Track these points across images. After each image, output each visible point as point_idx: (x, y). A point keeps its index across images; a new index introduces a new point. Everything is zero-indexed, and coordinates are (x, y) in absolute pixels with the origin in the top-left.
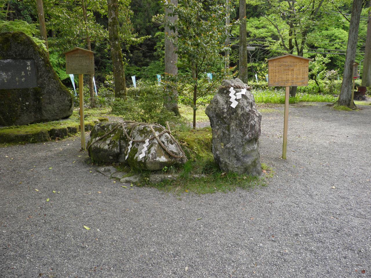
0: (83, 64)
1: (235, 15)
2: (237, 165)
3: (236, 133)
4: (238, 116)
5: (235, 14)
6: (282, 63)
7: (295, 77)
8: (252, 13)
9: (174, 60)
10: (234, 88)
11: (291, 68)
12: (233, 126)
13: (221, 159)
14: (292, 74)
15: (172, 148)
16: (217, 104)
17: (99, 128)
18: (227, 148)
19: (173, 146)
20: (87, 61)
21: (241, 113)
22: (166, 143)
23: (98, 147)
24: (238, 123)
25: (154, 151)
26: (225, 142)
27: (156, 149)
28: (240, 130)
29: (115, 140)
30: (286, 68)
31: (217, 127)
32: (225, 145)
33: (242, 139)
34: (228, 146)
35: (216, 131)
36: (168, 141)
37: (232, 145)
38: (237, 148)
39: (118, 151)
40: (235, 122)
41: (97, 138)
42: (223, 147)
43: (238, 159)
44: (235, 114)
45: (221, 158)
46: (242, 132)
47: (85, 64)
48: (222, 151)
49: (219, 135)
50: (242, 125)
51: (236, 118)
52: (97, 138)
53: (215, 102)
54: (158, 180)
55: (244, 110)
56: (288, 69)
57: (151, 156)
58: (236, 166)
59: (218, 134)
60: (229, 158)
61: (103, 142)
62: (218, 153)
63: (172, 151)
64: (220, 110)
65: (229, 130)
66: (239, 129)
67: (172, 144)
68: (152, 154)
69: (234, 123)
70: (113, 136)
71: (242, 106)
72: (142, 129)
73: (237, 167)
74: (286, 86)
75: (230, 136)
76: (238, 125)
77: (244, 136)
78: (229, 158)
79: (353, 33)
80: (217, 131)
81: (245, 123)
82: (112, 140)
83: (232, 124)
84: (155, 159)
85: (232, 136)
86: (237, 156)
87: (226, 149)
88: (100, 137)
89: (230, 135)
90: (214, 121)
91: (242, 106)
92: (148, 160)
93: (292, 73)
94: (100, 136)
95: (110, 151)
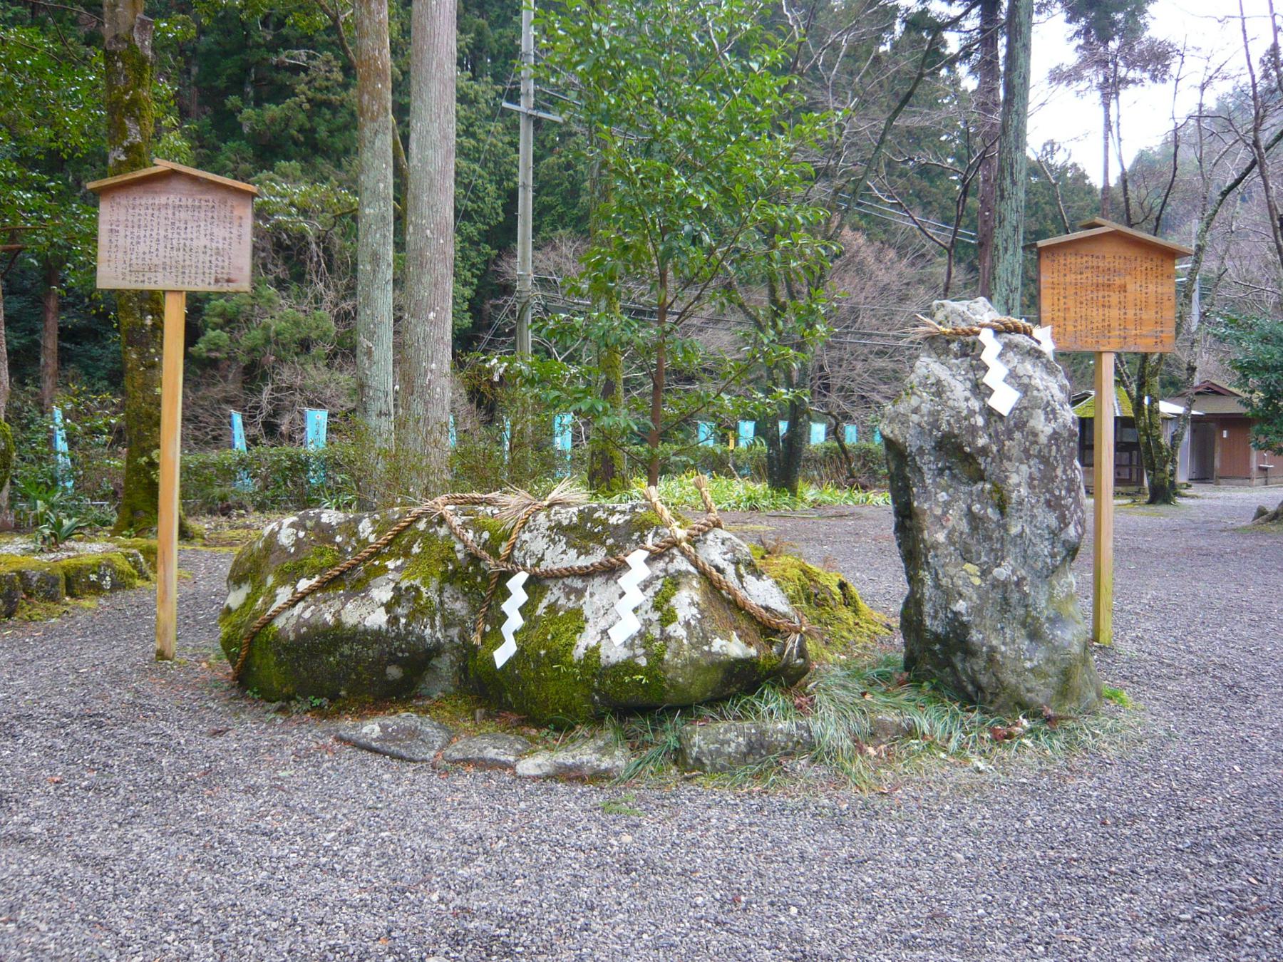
0: (195, 243)
1: (497, 214)
2: (1031, 660)
3: (1033, 517)
4: (1036, 442)
5: (500, 211)
6: (1085, 259)
7: (1131, 313)
8: (560, 209)
9: (442, 308)
10: (997, 332)
11: (1118, 281)
12: (1019, 485)
13: (975, 636)
14: (1122, 305)
15: (763, 593)
16: (939, 394)
17: (301, 534)
18: (996, 584)
19: (767, 583)
20: (215, 230)
21: (1048, 430)
22: (730, 569)
23: (325, 623)
24: (1037, 475)
25: (694, 611)
26: (984, 559)
27: (696, 598)
28: (1048, 503)
29: (417, 582)
30: (1100, 280)
31: (943, 496)
32: (984, 574)
33: (1053, 544)
34: (1002, 572)
35: (938, 511)
36: (736, 563)
37: (1014, 572)
38: (1033, 585)
39: (439, 635)
40: (1024, 468)
41: (303, 585)
42: (977, 581)
43: (1034, 635)
44: (1017, 435)
45: (973, 632)
46: (1055, 510)
47: (204, 241)
48: (980, 598)
49: (954, 529)
50: (1053, 481)
51: (1026, 451)
52: (303, 585)
53: (925, 386)
54: (731, 748)
55: (1056, 419)
56: (1109, 286)
57: (684, 634)
58: (1028, 665)
59: (950, 524)
60: (1002, 628)
61: (348, 598)
62: (961, 606)
63: (767, 609)
64: (958, 421)
65: (1002, 506)
66: (1042, 499)
67: (758, 574)
68: (687, 624)
69: (1017, 472)
70: (397, 569)
71: (1048, 402)
72: (575, 519)
73: (1031, 670)
74: (1102, 349)
75: (1006, 530)
76: (1036, 482)
77: (1061, 530)
78: (1002, 628)
79: (1007, 256)
80: (945, 513)
81: (1065, 472)
82: (404, 585)
83: (1014, 479)
84: (706, 648)
85: (1014, 530)
86: (1029, 620)
87: (994, 587)
88: (317, 578)
89: (1005, 528)
90: (925, 468)
91: (1048, 402)
92: (677, 655)
93: (1122, 299)
94: (321, 570)
95: (398, 634)
